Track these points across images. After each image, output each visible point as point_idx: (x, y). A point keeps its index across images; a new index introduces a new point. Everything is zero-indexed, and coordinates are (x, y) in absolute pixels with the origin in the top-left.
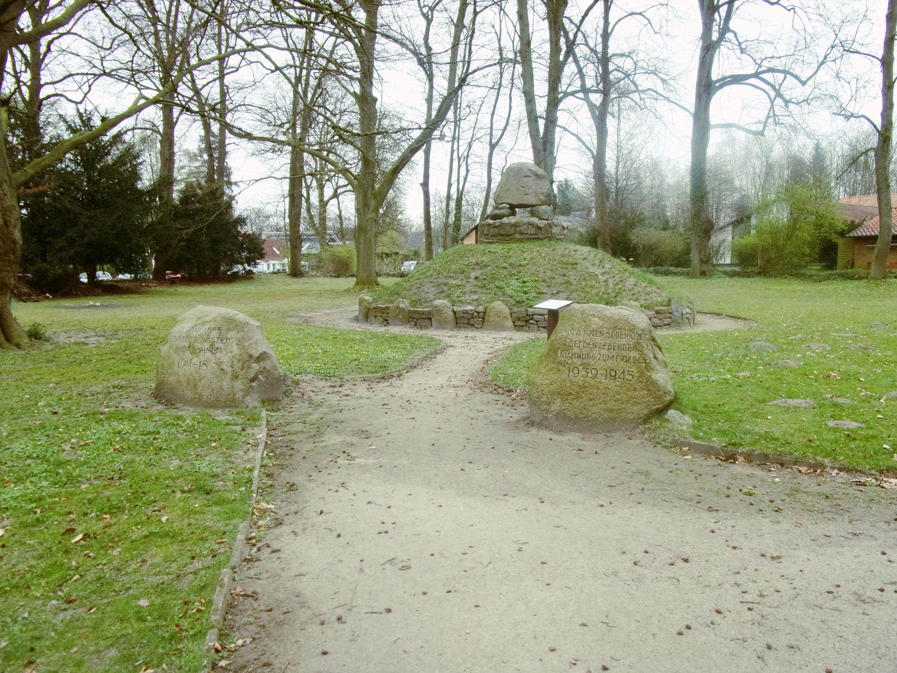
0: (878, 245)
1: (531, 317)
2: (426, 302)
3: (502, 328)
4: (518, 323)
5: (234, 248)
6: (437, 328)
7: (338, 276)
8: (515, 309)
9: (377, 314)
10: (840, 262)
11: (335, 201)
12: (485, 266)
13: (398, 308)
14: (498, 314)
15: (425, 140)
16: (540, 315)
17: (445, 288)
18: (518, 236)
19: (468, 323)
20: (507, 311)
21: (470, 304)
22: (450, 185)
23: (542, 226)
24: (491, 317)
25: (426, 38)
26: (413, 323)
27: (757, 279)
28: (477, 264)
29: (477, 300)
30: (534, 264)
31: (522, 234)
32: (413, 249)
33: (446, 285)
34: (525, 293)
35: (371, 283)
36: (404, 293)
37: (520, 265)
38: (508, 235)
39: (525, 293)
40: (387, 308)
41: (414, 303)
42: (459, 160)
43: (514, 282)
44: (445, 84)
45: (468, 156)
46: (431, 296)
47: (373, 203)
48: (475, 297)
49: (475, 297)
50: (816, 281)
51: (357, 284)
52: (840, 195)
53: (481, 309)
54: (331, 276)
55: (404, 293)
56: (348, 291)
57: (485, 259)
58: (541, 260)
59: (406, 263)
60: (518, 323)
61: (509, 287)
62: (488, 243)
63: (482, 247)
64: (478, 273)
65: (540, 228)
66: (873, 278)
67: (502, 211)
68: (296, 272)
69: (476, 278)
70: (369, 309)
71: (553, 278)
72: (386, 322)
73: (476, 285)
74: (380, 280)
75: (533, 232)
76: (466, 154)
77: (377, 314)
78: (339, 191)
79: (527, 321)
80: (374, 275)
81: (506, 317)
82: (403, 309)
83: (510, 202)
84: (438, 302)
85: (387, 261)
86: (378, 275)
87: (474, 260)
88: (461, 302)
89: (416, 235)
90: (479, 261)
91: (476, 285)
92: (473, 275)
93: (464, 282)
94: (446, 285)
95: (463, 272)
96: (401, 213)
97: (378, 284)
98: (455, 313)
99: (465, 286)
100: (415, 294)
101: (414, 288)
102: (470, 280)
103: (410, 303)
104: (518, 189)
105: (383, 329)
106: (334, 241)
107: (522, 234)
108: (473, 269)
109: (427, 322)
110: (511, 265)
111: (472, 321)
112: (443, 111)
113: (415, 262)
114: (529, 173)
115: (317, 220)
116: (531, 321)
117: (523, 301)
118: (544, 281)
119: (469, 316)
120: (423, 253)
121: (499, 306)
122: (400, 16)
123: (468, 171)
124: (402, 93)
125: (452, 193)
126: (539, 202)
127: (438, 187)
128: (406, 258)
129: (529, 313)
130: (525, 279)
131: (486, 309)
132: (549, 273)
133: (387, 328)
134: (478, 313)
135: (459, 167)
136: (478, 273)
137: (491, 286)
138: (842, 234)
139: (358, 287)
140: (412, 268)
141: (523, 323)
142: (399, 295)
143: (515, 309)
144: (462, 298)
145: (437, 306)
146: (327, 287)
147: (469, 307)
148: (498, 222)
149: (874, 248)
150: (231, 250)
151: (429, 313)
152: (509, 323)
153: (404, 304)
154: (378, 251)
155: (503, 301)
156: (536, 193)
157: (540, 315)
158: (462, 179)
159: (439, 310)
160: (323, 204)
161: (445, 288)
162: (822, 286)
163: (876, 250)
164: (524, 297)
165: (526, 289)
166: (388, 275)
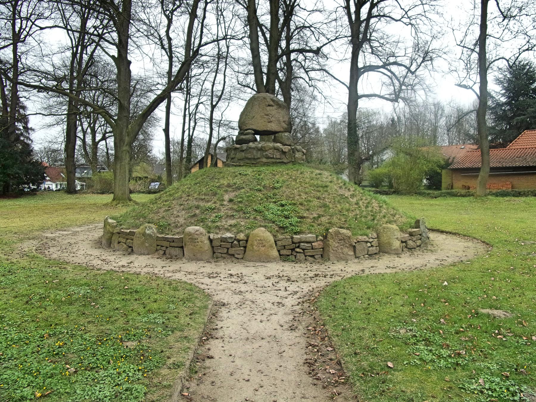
0: (481, 173)
1: (298, 244)
2: (176, 227)
3: (268, 259)
4: (284, 252)
5: (20, 172)
6: (190, 260)
7: (103, 193)
8: (280, 237)
9: (121, 239)
10: (444, 185)
11: (103, 142)
12: (239, 188)
13: (144, 234)
14: (262, 242)
15: (165, 96)
16: (307, 242)
17: (197, 212)
18: (264, 160)
19: (227, 253)
20: (272, 239)
21: (228, 230)
22: (184, 132)
23: (287, 150)
24: (254, 246)
25: (167, 32)
26: (161, 252)
27: (393, 196)
28: (229, 186)
29: (235, 226)
30: (288, 187)
31: (268, 158)
32: (157, 175)
33: (197, 207)
34: (287, 217)
35: (123, 199)
36: (151, 216)
37: (274, 188)
38: (254, 159)
39: (287, 217)
40: (132, 234)
41: (161, 228)
42: (190, 116)
43: (272, 205)
44: (182, 51)
45: (195, 113)
46: (181, 220)
47: (127, 139)
48: (232, 222)
49: (232, 222)
50: (432, 197)
51: (114, 200)
52: (443, 140)
53: (242, 236)
54: (98, 193)
55: (151, 216)
56: (106, 205)
57: (238, 181)
58: (294, 183)
59: (153, 184)
60: (284, 252)
61: (268, 210)
62: (235, 166)
63: (231, 169)
64: (232, 195)
65: (284, 153)
66: (479, 196)
67: (247, 136)
68: (71, 190)
69: (231, 201)
70: (113, 234)
71: (310, 201)
72: (130, 251)
73: (231, 209)
74: (132, 196)
75: (278, 157)
76: (194, 112)
77: (121, 239)
78: (107, 135)
79: (293, 250)
80: (127, 192)
81: (271, 246)
82: (150, 235)
83: (255, 128)
84: (191, 229)
85: (139, 182)
86: (131, 192)
87: (225, 182)
88: (217, 227)
89: (160, 165)
90: (231, 182)
91: (231, 209)
92: (226, 197)
93: (218, 205)
94: (197, 207)
95: (215, 194)
96: (149, 152)
97: (130, 200)
98: (211, 241)
99: (219, 210)
100: (163, 217)
101: (161, 211)
102: (225, 203)
103: (158, 229)
104: (262, 117)
105: (124, 261)
106: (104, 169)
107: (268, 158)
108: (226, 191)
109: (177, 251)
110: (264, 187)
111: (231, 251)
112: (178, 80)
113: (158, 183)
114: (272, 103)
115: (90, 155)
116: (298, 250)
117: (287, 227)
118: (301, 204)
119: (229, 245)
120: (164, 177)
121: (263, 233)
122: (148, 10)
123: (196, 123)
124: (147, 63)
125: (185, 138)
126: (282, 130)
127: (176, 135)
128: (153, 181)
129: (295, 241)
130: (283, 202)
131: (248, 236)
132: (304, 196)
133: (133, 258)
134: (239, 241)
135: (190, 120)
136: (232, 195)
137: (249, 209)
138: (442, 167)
139: (115, 203)
140: (157, 187)
141: (288, 252)
142: (145, 218)
143: (280, 237)
144: (219, 224)
145: (190, 234)
146: (92, 202)
147: (228, 235)
148: (245, 146)
149: (478, 175)
150: (18, 173)
151: (181, 240)
152: (275, 253)
153: (152, 230)
154: (133, 176)
155: (265, 227)
156: (279, 121)
157: (307, 242)
158: (191, 128)
159: (193, 238)
160: (95, 144)
161: (197, 212)
162: (433, 202)
163: (479, 178)
164: (287, 222)
165: (286, 213)
166: (139, 192)
